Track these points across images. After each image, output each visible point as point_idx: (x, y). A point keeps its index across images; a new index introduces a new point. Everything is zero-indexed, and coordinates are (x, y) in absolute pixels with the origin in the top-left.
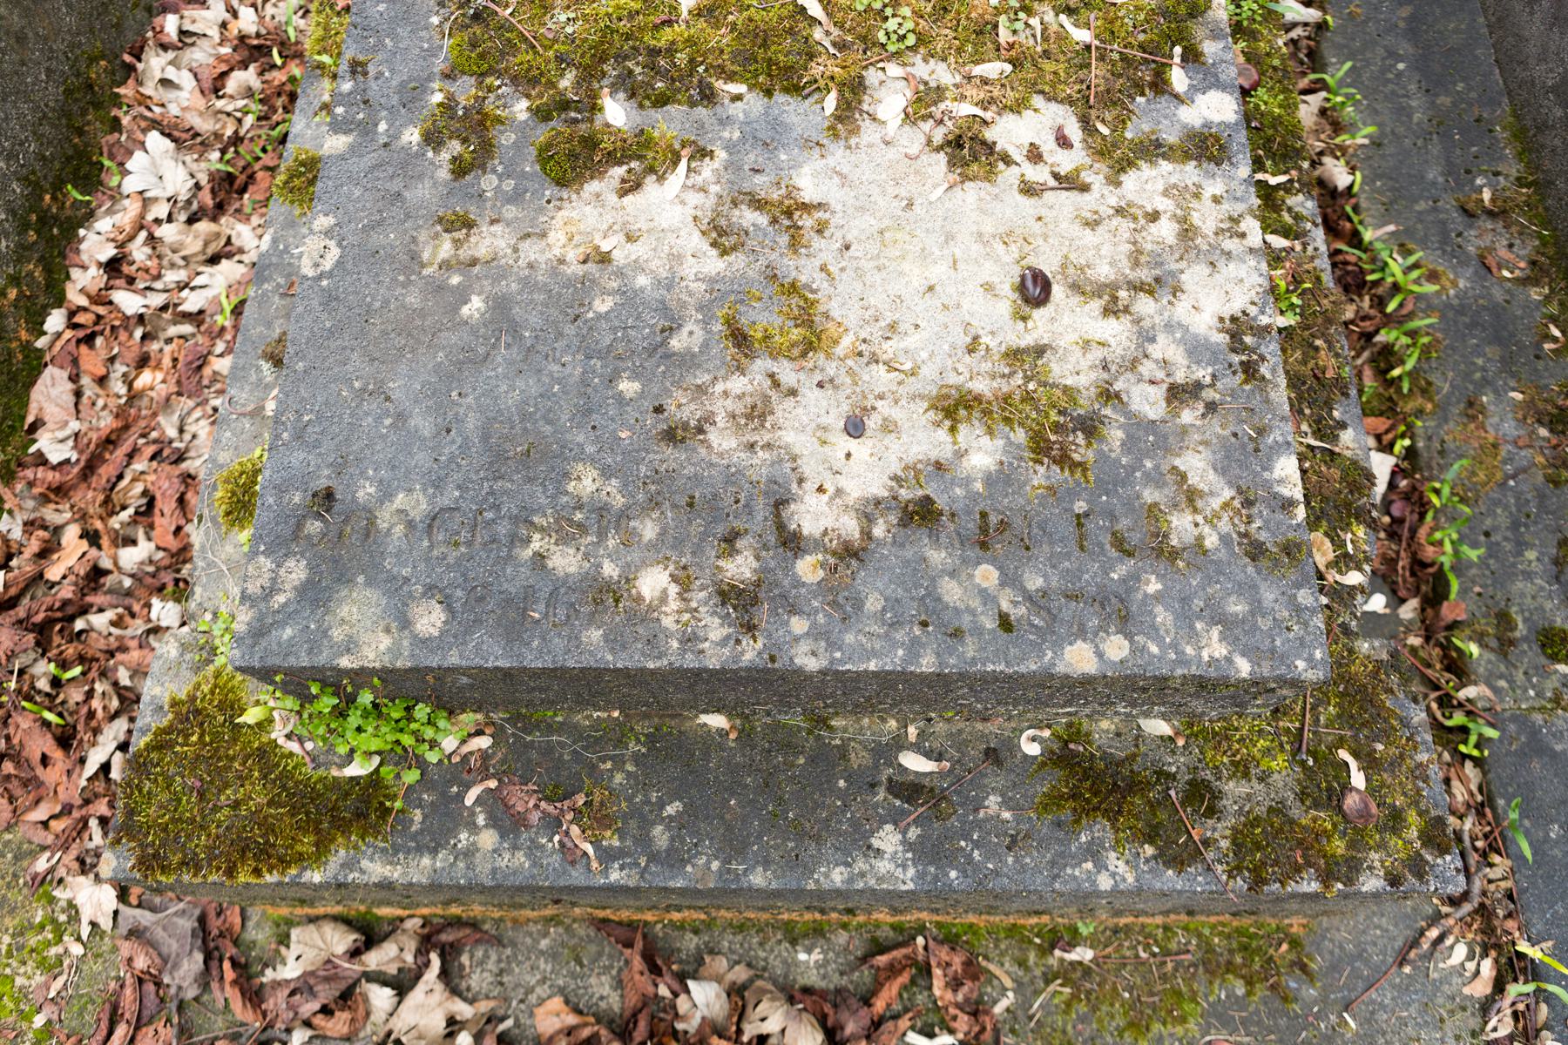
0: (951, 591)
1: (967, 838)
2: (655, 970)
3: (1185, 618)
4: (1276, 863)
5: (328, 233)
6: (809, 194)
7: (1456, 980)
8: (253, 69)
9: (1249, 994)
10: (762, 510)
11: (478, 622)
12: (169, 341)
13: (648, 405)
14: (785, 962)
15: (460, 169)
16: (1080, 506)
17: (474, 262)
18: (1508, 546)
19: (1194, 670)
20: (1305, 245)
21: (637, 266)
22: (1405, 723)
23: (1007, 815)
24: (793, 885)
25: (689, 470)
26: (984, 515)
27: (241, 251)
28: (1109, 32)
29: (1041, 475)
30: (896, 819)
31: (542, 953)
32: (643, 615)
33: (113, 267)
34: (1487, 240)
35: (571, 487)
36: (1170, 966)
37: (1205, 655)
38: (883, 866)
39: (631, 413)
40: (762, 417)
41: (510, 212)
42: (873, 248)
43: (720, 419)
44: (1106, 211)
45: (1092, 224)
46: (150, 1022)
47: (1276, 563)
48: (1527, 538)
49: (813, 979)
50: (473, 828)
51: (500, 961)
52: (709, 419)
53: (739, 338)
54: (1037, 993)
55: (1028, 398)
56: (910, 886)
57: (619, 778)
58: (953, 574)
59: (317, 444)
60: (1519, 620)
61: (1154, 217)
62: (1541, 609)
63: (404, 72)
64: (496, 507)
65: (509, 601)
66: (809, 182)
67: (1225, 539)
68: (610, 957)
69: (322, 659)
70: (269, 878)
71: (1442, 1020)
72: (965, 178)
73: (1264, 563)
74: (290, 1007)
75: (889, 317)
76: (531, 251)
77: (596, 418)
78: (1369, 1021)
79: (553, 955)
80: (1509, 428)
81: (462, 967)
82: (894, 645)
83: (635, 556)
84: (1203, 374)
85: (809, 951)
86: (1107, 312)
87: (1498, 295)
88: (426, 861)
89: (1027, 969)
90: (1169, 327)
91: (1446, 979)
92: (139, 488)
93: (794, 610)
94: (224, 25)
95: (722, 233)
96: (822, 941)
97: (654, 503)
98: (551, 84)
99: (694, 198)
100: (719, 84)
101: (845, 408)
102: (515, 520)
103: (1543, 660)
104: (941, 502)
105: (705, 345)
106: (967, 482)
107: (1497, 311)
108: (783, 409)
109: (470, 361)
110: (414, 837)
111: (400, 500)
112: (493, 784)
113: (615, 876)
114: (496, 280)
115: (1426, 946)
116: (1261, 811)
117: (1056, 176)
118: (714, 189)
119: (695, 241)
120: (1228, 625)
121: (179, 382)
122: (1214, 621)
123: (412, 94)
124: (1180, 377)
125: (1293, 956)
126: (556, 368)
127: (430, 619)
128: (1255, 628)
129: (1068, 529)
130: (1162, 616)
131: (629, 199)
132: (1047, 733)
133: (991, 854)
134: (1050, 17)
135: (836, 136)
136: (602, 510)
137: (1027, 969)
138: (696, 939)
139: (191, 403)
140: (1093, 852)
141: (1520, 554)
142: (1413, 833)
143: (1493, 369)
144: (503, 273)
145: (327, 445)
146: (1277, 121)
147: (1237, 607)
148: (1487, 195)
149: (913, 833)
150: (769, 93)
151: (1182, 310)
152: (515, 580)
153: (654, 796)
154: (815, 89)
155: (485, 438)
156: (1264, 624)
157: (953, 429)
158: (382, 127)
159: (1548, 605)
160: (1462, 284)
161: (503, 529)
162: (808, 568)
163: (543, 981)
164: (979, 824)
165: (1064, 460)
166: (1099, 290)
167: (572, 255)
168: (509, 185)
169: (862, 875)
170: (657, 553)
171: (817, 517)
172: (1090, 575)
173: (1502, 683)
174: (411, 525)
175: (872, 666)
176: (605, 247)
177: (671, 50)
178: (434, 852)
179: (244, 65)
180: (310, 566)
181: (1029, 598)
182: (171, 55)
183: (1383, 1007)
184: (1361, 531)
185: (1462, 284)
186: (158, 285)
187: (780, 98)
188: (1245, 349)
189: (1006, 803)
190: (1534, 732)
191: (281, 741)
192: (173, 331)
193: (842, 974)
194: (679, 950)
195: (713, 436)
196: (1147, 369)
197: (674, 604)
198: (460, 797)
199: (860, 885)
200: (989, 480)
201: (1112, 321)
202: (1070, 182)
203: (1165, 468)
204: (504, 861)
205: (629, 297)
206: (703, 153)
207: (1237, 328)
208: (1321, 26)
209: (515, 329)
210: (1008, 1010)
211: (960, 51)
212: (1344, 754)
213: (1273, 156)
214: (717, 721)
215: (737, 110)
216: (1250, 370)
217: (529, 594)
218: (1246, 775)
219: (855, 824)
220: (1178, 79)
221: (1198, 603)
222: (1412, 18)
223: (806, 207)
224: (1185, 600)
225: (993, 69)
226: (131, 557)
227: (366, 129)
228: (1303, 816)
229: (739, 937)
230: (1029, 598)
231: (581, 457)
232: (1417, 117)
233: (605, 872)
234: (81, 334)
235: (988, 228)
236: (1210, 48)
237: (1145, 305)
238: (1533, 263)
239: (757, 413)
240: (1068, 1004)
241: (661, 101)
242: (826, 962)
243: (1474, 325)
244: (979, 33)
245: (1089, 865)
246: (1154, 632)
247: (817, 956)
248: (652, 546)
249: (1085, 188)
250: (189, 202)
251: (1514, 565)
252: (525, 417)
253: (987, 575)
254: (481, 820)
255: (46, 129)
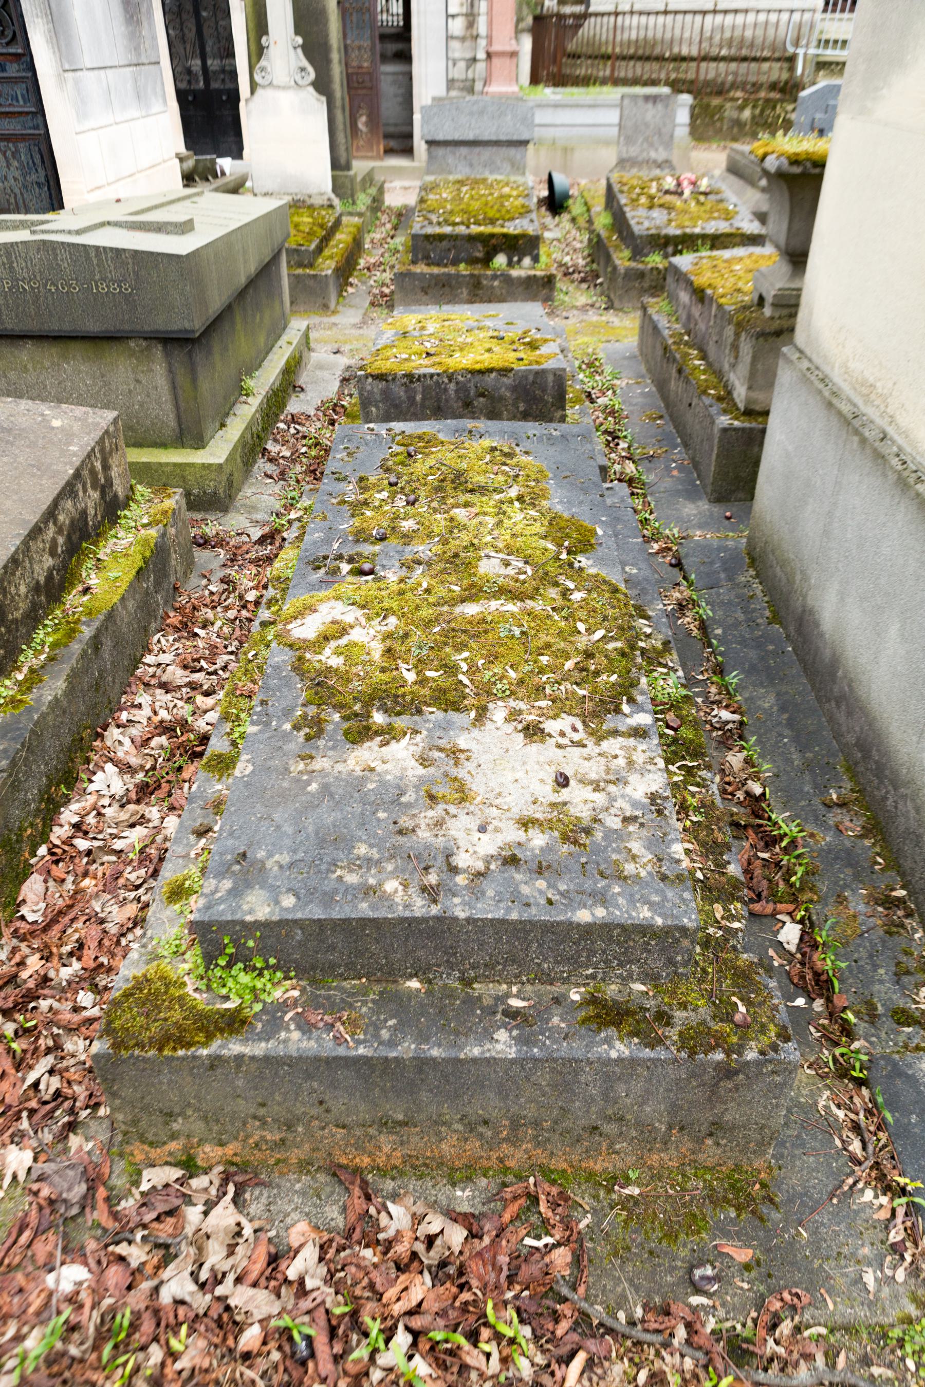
0: (525, 890)
1: (543, 1034)
2: (368, 1198)
3: (632, 901)
4: (701, 1045)
5: (248, 761)
6: (463, 746)
7: (868, 1210)
8: (164, 737)
9: (738, 1216)
10: (441, 859)
11: (311, 901)
12: (103, 864)
13: (391, 821)
14: (448, 1197)
15: (308, 738)
16: (583, 860)
17: (313, 771)
18: (868, 967)
19: (636, 922)
20: (708, 791)
21: (387, 772)
22: (766, 987)
23: (563, 1025)
24: (453, 1055)
25: (409, 845)
26: (540, 862)
27: (149, 821)
28: (595, 691)
29: (565, 848)
30: (505, 1026)
31: (296, 1192)
32: (387, 898)
33: (77, 827)
34: (839, 818)
35: (355, 851)
36: (687, 1198)
37: (641, 916)
38: (499, 1047)
39: (383, 825)
40: (441, 825)
41: (330, 753)
42: (491, 766)
43: (423, 826)
44: (593, 754)
45: (589, 759)
46: (43, 1232)
47: (673, 881)
48: (878, 962)
49: (465, 1208)
50: (288, 1030)
51: (269, 1197)
52: (418, 826)
53: (432, 797)
54: (606, 1216)
55: (559, 820)
56: (514, 1056)
57: (364, 1009)
58: (526, 883)
59: (239, 837)
60: (879, 1005)
61: (616, 757)
62: (890, 999)
63: (284, 704)
64: (321, 860)
65: (325, 894)
66: (463, 742)
67: (650, 873)
68: (339, 1194)
69: (238, 917)
70: (181, 1053)
71: (861, 1233)
72: (532, 742)
73: (667, 882)
74: (138, 1214)
75: (498, 790)
76: (339, 767)
77: (367, 826)
78: (815, 1233)
79: (303, 1193)
80: (861, 908)
81: (245, 1201)
82: (499, 908)
83: (384, 876)
84: (639, 813)
85: (463, 1190)
86: (594, 790)
87: (848, 844)
88: (263, 1044)
89: (599, 1201)
90: (623, 796)
91: (862, 1210)
92: (76, 936)
93: (454, 895)
94: (149, 718)
95: (425, 760)
96: (471, 1185)
97: (392, 857)
98: (350, 708)
99: (412, 748)
100: (424, 708)
101: (478, 822)
102: (329, 864)
103: (895, 1026)
104: (520, 856)
105: (417, 800)
106: (532, 850)
107: (848, 852)
108: (450, 823)
109: (311, 806)
110: (257, 1034)
111: (277, 857)
112: (300, 1010)
113: (361, 1051)
114: (324, 777)
115: (846, 1188)
116: (694, 1024)
117: (572, 742)
118: (421, 745)
119: (413, 763)
120: (652, 905)
121: (105, 885)
122: (644, 903)
123: (287, 712)
124: (628, 814)
125: (763, 1193)
126: (349, 809)
127: (289, 901)
128: (664, 906)
129: (578, 867)
130: (621, 901)
131: (383, 749)
132: (582, 989)
133: (555, 1041)
134: (569, 686)
135: (475, 726)
136: (369, 859)
137: (599, 1201)
138: (393, 1184)
139: (109, 897)
140: (608, 1041)
141: (875, 971)
142: (773, 1034)
143: (849, 879)
144: (327, 775)
145: (244, 837)
146: (691, 741)
147: (655, 898)
148: (834, 796)
149: (515, 1033)
150: (446, 711)
151: (629, 790)
152: (328, 886)
153: (382, 1017)
154: (467, 709)
155: (317, 834)
156: (668, 905)
157: (526, 831)
158: (274, 723)
159: (895, 997)
160: (828, 839)
161: (324, 867)
162: (461, 880)
163: (296, 1209)
164: (549, 1029)
165: (575, 842)
166: (591, 783)
167: (358, 768)
168: (330, 744)
169: (489, 1050)
170: (393, 875)
171: (465, 861)
172: (588, 885)
173: (874, 1039)
174: (281, 867)
175: (490, 916)
176: (373, 765)
177: (404, 695)
178: (268, 1040)
179: (160, 735)
180: (234, 882)
181: (560, 893)
182: (121, 730)
183: (822, 1224)
184: (739, 905)
185: (828, 839)
186: (100, 836)
187: (450, 713)
188: (657, 805)
189: (562, 1020)
190: (895, 1064)
191: (191, 992)
192: (106, 858)
193: (483, 1204)
194: (382, 1190)
195: (420, 833)
196: (613, 811)
197: (400, 893)
198: (282, 1018)
199: (488, 1055)
200: (542, 849)
201: (597, 794)
202: (580, 744)
203: (622, 846)
204: (304, 1044)
205: (383, 783)
206: (417, 732)
207: (653, 797)
208: (741, 723)
209: (331, 795)
210: (588, 1226)
211: (529, 697)
212: (734, 999)
213: (690, 755)
214: (414, 984)
215: (432, 717)
216: (660, 812)
217: (336, 891)
218: (685, 1008)
219: (485, 1029)
220: (626, 708)
221: (637, 896)
222: (788, 719)
223: (462, 751)
224: (632, 895)
225: (543, 703)
226: (66, 973)
227: (267, 724)
228: (716, 1026)
229: (420, 1182)
230: (560, 893)
231: (360, 840)
232: (796, 763)
233: (356, 1048)
234: (55, 858)
235: (542, 759)
236: (640, 698)
237: (612, 788)
238: (863, 827)
239: (439, 823)
240: (626, 1222)
241: (399, 714)
242: (474, 1197)
243: (836, 858)
244: (537, 690)
245: (606, 1047)
246: (618, 907)
247: (468, 1193)
248: (391, 872)
249: (584, 746)
250: (122, 797)
251: (873, 977)
252: (334, 826)
253: (541, 884)
254: (292, 1027)
255: (61, 755)
